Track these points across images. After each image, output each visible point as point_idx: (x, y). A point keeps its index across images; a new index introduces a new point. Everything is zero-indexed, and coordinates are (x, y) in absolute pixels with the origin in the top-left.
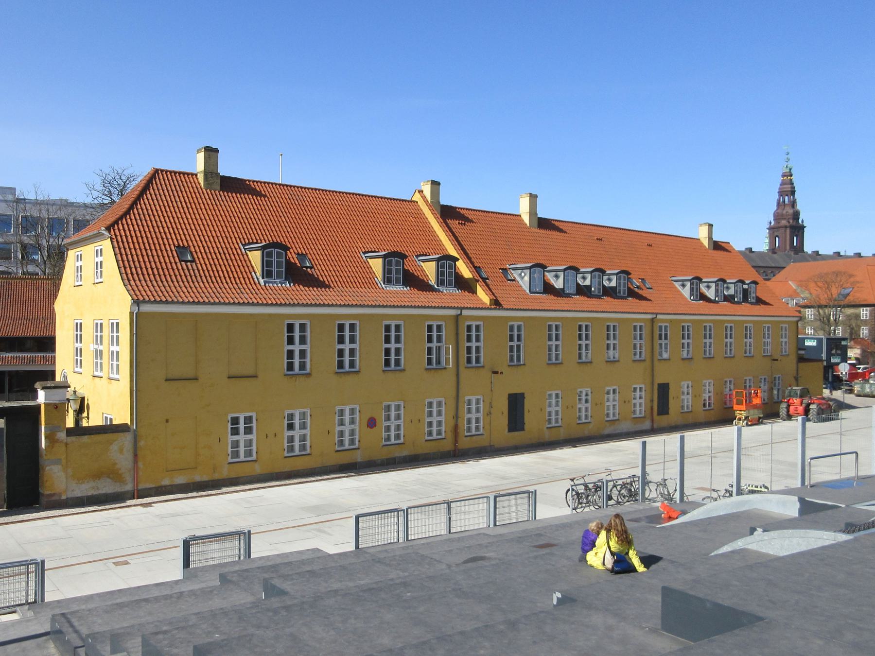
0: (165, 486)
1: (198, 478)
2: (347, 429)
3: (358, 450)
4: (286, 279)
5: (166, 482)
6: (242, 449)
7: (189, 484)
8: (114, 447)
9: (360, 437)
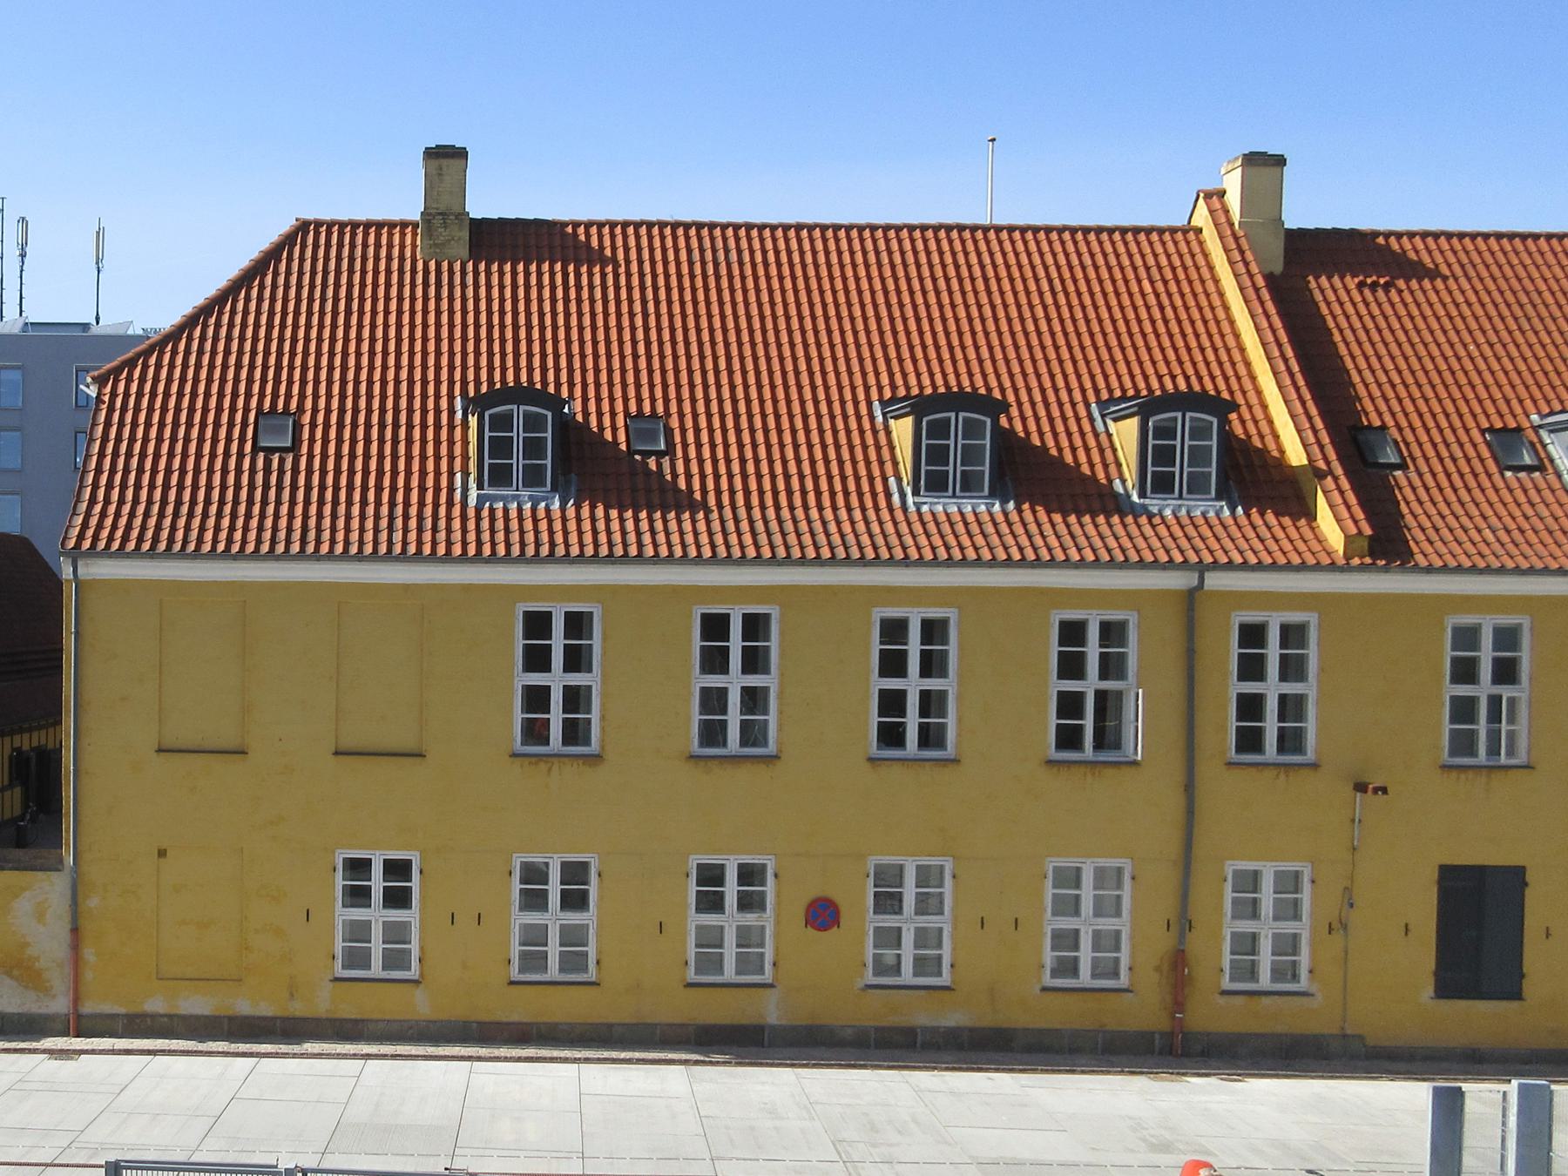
0: (153, 1016)
1: (244, 1007)
2: (1267, 929)
3: (768, 991)
4: (554, 489)
5: (156, 1005)
6: (1265, 958)
7: (219, 1017)
8: (23, 906)
9: (777, 950)
